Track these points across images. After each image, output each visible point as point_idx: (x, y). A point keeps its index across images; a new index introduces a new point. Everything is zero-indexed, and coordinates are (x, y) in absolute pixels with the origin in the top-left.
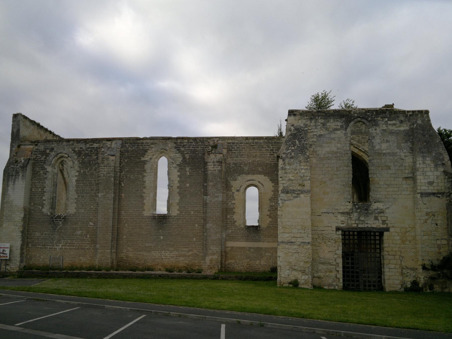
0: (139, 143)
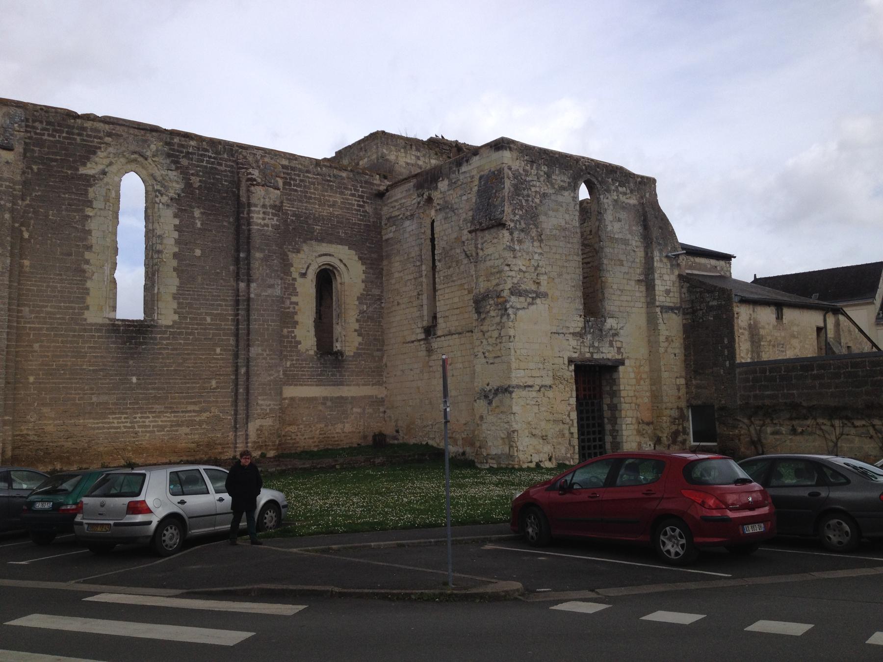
0: (73, 127)
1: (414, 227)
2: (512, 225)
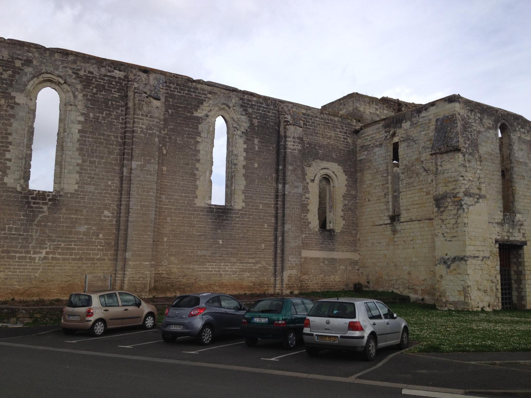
0: (191, 88)
1: (382, 152)
2: (465, 150)
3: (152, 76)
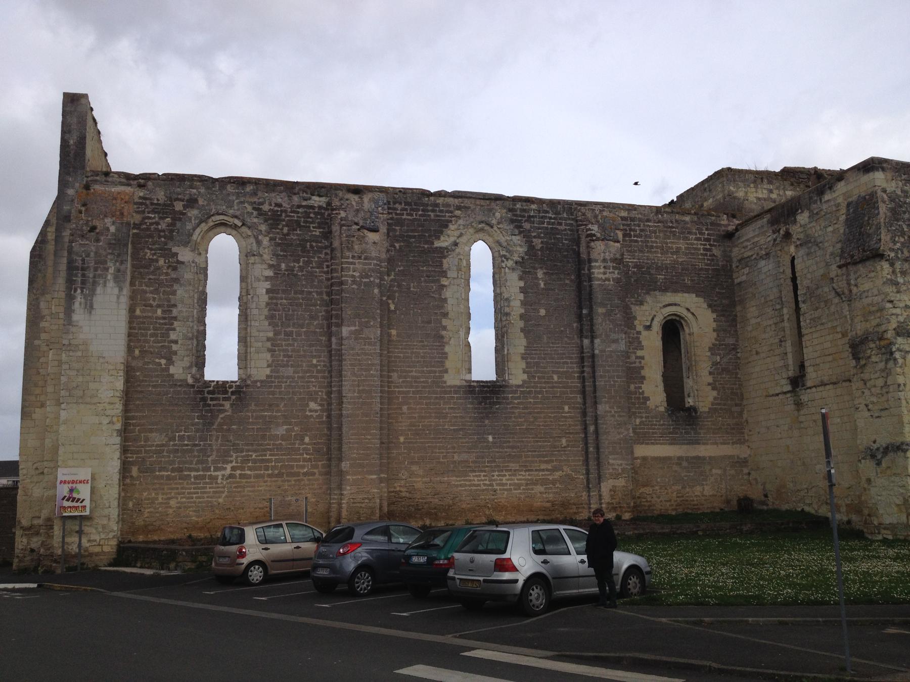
0: (427, 205)
1: (770, 267)
3: (366, 198)
